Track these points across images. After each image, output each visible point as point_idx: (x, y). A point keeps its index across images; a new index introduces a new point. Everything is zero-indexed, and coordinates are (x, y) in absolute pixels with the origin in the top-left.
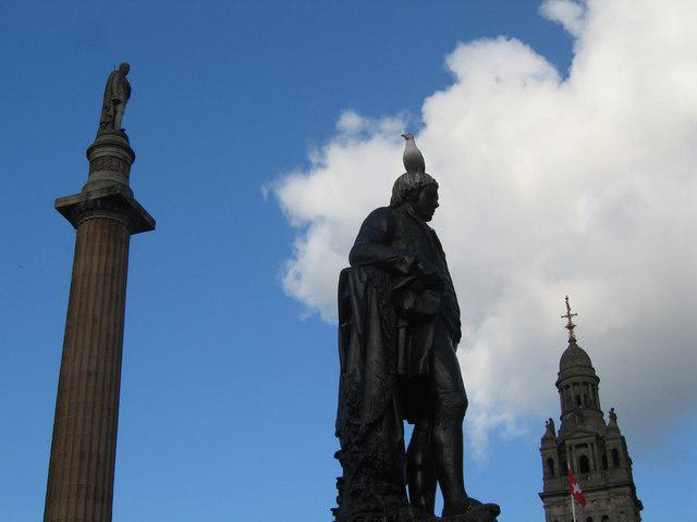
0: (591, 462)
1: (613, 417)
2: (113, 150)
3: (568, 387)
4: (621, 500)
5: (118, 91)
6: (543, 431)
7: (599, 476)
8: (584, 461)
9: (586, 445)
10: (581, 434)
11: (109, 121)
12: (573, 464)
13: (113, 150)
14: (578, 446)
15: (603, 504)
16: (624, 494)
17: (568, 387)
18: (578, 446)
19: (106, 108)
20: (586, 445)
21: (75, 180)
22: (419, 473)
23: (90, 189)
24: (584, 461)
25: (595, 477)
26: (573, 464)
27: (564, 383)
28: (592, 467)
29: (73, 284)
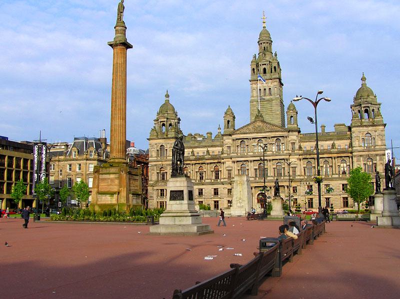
0: (267, 70)
1: (276, 55)
2: (121, 26)
3: (261, 44)
4: (276, 83)
5: (121, 9)
6: (252, 59)
7: (269, 75)
8: (265, 69)
9: (265, 64)
10: (264, 61)
11: (120, 19)
12: (261, 68)
13: (121, 26)
14: (263, 65)
15: (270, 84)
16: (277, 81)
17: (261, 44)
18: (263, 65)
19: (118, 14)
20: (265, 64)
21: (111, 36)
22: (206, 258)
23: (116, 40)
24: (265, 69)
25: (268, 75)
26: (261, 68)
27: (260, 42)
28: (267, 72)
29: (114, 65)
